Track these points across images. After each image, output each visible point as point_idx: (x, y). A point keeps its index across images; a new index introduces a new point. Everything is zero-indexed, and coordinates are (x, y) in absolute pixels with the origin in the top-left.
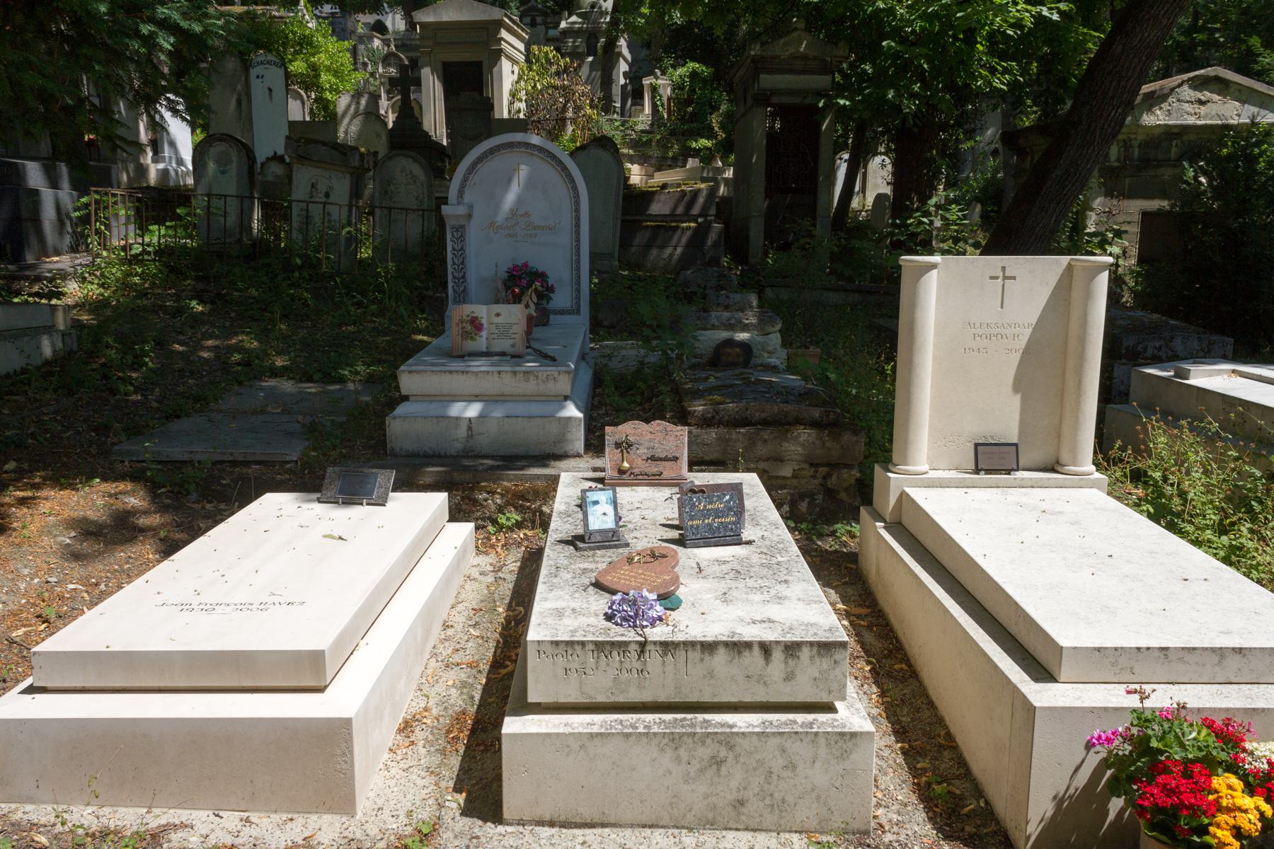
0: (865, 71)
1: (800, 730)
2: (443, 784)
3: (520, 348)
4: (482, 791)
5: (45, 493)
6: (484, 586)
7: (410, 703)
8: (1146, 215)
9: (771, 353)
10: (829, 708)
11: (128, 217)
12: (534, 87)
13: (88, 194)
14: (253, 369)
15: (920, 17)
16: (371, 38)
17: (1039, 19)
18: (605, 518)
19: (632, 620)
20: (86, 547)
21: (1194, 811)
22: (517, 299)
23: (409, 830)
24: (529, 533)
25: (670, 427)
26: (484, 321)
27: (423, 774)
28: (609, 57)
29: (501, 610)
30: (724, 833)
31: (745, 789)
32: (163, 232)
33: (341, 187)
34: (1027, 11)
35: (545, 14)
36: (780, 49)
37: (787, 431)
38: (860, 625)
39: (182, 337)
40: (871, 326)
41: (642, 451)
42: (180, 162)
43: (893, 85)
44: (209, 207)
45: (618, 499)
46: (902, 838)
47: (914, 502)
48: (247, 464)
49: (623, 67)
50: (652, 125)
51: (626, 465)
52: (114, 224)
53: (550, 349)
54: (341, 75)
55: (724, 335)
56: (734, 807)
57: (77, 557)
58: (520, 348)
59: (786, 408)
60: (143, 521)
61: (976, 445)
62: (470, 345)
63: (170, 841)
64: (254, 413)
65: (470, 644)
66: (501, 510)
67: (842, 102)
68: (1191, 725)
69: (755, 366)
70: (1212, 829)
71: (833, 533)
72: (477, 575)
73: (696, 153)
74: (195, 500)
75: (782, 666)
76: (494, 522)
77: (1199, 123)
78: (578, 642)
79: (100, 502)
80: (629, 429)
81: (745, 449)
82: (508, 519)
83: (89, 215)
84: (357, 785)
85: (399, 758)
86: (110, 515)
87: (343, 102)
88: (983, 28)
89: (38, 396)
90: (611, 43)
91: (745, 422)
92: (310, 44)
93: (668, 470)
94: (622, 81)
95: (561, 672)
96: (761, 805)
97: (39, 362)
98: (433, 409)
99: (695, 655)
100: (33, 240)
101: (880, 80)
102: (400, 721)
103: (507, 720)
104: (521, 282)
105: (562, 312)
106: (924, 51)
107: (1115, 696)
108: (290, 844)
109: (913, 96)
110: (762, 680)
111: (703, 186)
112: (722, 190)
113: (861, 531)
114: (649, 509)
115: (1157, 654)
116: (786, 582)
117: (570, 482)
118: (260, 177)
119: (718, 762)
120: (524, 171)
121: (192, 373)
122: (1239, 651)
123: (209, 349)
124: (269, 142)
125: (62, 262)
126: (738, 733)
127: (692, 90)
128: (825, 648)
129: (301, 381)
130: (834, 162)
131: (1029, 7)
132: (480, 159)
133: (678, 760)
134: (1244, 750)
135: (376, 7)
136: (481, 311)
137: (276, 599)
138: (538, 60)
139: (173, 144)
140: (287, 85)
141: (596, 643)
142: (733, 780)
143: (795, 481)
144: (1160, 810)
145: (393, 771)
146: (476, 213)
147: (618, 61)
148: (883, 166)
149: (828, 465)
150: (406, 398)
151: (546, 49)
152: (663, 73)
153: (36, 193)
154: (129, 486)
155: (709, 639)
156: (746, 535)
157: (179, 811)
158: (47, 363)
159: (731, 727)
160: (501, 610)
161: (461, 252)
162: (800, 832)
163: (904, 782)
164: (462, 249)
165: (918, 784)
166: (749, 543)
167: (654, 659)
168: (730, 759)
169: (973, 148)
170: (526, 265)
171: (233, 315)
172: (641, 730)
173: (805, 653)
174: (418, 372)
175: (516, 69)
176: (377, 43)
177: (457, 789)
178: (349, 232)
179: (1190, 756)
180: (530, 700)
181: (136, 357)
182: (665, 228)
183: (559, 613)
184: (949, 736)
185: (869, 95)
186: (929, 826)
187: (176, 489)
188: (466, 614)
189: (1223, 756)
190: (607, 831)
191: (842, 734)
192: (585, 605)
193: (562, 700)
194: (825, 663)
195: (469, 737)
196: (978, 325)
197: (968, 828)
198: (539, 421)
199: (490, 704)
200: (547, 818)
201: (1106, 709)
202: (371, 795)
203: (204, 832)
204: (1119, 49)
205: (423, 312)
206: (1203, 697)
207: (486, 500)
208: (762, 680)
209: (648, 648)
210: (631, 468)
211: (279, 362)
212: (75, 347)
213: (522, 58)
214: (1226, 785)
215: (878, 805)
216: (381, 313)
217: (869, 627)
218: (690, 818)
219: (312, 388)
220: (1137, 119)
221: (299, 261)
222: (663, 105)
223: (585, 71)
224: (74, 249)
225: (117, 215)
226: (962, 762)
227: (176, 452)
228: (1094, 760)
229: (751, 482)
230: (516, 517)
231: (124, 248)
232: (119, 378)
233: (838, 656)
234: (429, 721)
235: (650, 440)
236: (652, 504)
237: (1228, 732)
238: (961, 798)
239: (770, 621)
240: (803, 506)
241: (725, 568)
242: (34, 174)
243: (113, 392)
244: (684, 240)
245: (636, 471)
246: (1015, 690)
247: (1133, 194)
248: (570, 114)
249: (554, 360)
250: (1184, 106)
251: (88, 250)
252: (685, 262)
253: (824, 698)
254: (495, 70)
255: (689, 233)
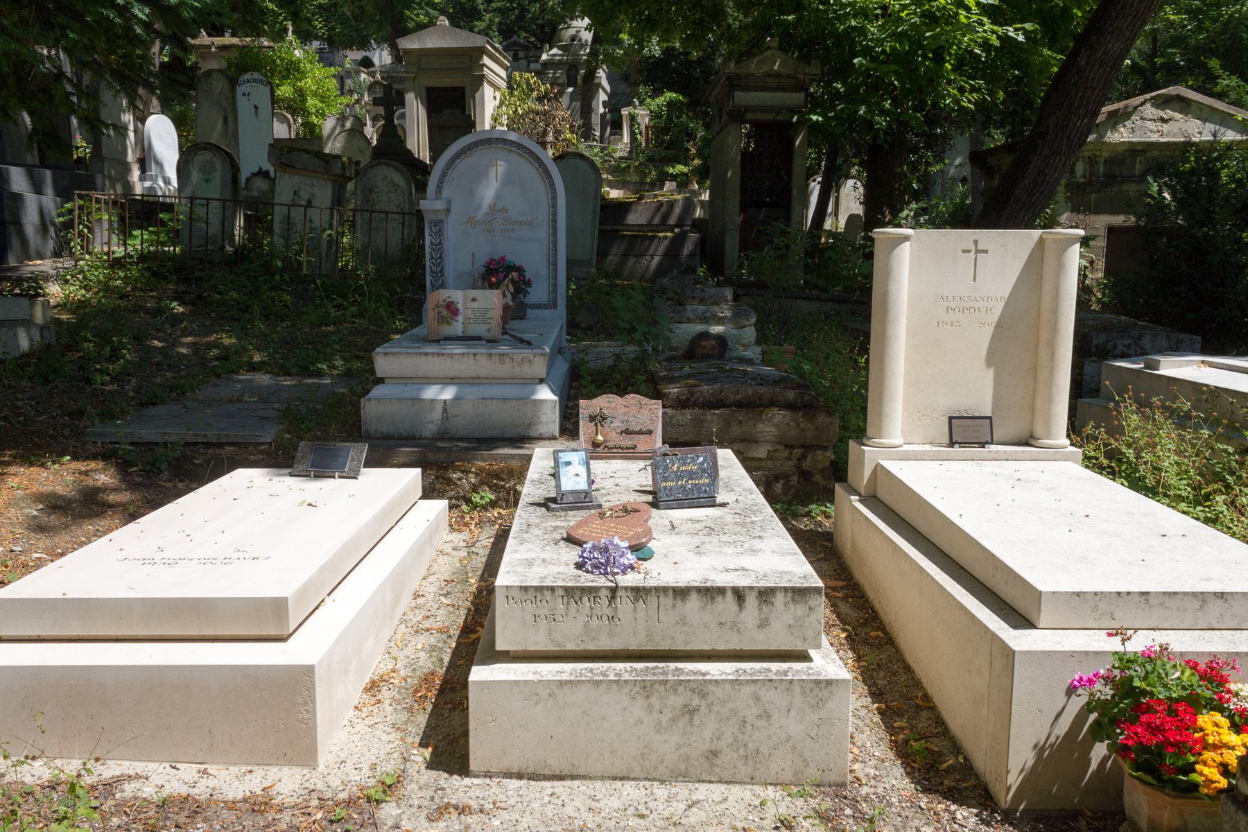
0: (838, 90)
1: (774, 677)
2: (409, 740)
3: (496, 332)
4: (448, 746)
5: (13, 469)
6: (456, 560)
7: (377, 665)
8: (1111, 230)
9: (746, 346)
10: (804, 657)
11: (110, 222)
12: (515, 112)
13: (73, 200)
14: (230, 362)
15: (889, 36)
16: (358, 73)
17: (1005, 39)
18: (578, 479)
19: (604, 566)
20: (53, 519)
21: (1180, 749)
22: (492, 286)
23: (373, 782)
24: (503, 512)
25: (645, 400)
26: (460, 306)
27: (389, 730)
28: (588, 89)
29: (473, 581)
30: (697, 785)
31: (718, 739)
32: (145, 237)
33: (323, 194)
34: (993, 32)
35: (527, 49)
36: (753, 66)
37: (762, 412)
38: (836, 597)
39: (161, 334)
40: (842, 302)
41: (616, 424)
42: (167, 181)
43: (864, 101)
44: (191, 212)
45: (592, 467)
46: (880, 790)
47: (888, 472)
48: (220, 445)
49: (603, 97)
50: (630, 152)
51: (600, 438)
52: (97, 230)
53: (526, 336)
54: (323, 92)
55: (700, 328)
56: (707, 758)
57: (41, 528)
58: (496, 332)
59: (762, 390)
60: (113, 498)
61: (950, 418)
62: (447, 330)
63: (123, 791)
64: (230, 401)
65: (441, 611)
66: (475, 489)
67: (814, 118)
68: (1175, 666)
69: (731, 359)
70: (1198, 767)
71: (808, 514)
72: (450, 550)
73: (674, 178)
74: (162, 473)
75: (756, 613)
76: (468, 501)
77: (1162, 140)
78: (547, 587)
79: (70, 478)
80: (605, 403)
81: (720, 430)
82: (482, 498)
83: (72, 220)
84: (319, 729)
85: (364, 715)
86: (80, 491)
87: (328, 125)
88: (951, 47)
89: (13, 384)
90: (591, 74)
91: (716, 403)
92: (298, 70)
93: (642, 444)
94: (602, 110)
95: (530, 618)
96: (735, 756)
97: (17, 354)
98: (408, 391)
99: (667, 601)
100: (15, 243)
101: (851, 97)
102: (367, 680)
103: (475, 669)
104: (496, 272)
105: (539, 306)
106: (894, 67)
107: (1099, 642)
108: (248, 794)
109: (883, 112)
110: (736, 627)
111: (679, 197)
112: (698, 213)
113: (835, 511)
114: (623, 478)
115: (1137, 598)
116: (760, 537)
117: (540, 458)
118: (245, 192)
119: (690, 711)
120: (501, 166)
121: (170, 366)
122: (1221, 595)
123: (188, 345)
124: (253, 158)
125: (44, 265)
126: (710, 681)
127: (670, 119)
128: (799, 593)
129: (278, 375)
130: (807, 186)
131: (996, 28)
132: (458, 155)
133: (650, 708)
134: (1229, 691)
135: (363, 44)
136: (458, 296)
137: (241, 555)
138: (519, 86)
139: (160, 165)
140: (273, 108)
141: (566, 589)
142: (707, 729)
143: (770, 463)
144: (1145, 749)
145: (358, 727)
146: (454, 209)
147: (597, 91)
148: (855, 188)
149: (803, 446)
150: (381, 381)
151: (527, 75)
152: (641, 103)
153: (18, 198)
154: (101, 465)
155: (682, 584)
156: (719, 499)
157: (134, 763)
158: (24, 355)
159: (704, 674)
160: (473, 581)
161: (439, 246)
162: (775, 785)
163: (881, 739)
164: (440, 243)
165: (895, 742)
166: (723, 505)
167: (625, 605)
168: (702, 708)
169: (942, 171)
170: (503, 259)
171: (213, 315)
172: (612, 677)
173: (780, 599)
174: (393, 354)
175: (498, 95)
176: (363, 76)
177: (423, 744)
178: (330, 235)
179: (1174, 695)
180: (498, 648)
181: (113, 350)
182: (643, 237)
183: (530, 563)
184: (926, 697)
185: (842, 110)
186: (907, 780)
187: (148, 468)
188: (437, 584)
189: (1208, 694)
190: (576, 783)
191: (818, 682)
192: (555, 556)
193: (531, 648)
194: (800, 610)
195: (437, 696)
196: (950, 298)
197: (946, 782)
198: (515, 403)
199: (459, 666)
200: (515, 770)
201: (1087, 653)
202: (334, 748)
203: (159, 784)
204: (1084, 62)
205: (402, 313)
206: (1184, 642)
207: (460, 479)
208: (736, 627)
209: (619, 593)
210: (605, 441)
211: (257, 358)
212: (54, 342)
213: (503, 85)
214: (1211, 723)
215: (855, 760)
216: (361, 315)
217: (845, 599)
218: (662, 770)
219: (287, 382)
220: (1101, 136)
221: (279, 264)
222: (641, 133)
223: (565, 100)
224: (57, 254)
225: (100, 220)
226: (940, 721)
227: (149, 434)
228: (1078, 702)
229: (726, 457)
230: (490, 496)
231: (108, 254)
232: (97, 370)
233: (812, 603)
234: (396, 682)
235: (625, 414)
236: (626, 474)
237: (1213, 673)
238: (940, 754)
239: (743, 569)
240: (778, 487)
241: (699, 526)
242: (18, 180)
243: (89, 381)
244: (661, 249)
245: (610, 444)
246: (994, 637)
247: (1099, 210)
248: (550, 138)
249: (529, 343)
250: (1149, 125)
251: (71, 254)
252: (662, 271)
253: (798, 646)
254: (477, 95)
255: (666, 243)
